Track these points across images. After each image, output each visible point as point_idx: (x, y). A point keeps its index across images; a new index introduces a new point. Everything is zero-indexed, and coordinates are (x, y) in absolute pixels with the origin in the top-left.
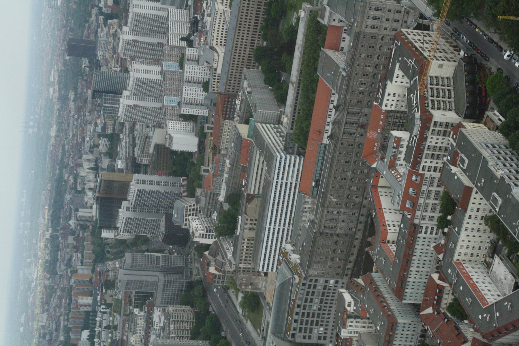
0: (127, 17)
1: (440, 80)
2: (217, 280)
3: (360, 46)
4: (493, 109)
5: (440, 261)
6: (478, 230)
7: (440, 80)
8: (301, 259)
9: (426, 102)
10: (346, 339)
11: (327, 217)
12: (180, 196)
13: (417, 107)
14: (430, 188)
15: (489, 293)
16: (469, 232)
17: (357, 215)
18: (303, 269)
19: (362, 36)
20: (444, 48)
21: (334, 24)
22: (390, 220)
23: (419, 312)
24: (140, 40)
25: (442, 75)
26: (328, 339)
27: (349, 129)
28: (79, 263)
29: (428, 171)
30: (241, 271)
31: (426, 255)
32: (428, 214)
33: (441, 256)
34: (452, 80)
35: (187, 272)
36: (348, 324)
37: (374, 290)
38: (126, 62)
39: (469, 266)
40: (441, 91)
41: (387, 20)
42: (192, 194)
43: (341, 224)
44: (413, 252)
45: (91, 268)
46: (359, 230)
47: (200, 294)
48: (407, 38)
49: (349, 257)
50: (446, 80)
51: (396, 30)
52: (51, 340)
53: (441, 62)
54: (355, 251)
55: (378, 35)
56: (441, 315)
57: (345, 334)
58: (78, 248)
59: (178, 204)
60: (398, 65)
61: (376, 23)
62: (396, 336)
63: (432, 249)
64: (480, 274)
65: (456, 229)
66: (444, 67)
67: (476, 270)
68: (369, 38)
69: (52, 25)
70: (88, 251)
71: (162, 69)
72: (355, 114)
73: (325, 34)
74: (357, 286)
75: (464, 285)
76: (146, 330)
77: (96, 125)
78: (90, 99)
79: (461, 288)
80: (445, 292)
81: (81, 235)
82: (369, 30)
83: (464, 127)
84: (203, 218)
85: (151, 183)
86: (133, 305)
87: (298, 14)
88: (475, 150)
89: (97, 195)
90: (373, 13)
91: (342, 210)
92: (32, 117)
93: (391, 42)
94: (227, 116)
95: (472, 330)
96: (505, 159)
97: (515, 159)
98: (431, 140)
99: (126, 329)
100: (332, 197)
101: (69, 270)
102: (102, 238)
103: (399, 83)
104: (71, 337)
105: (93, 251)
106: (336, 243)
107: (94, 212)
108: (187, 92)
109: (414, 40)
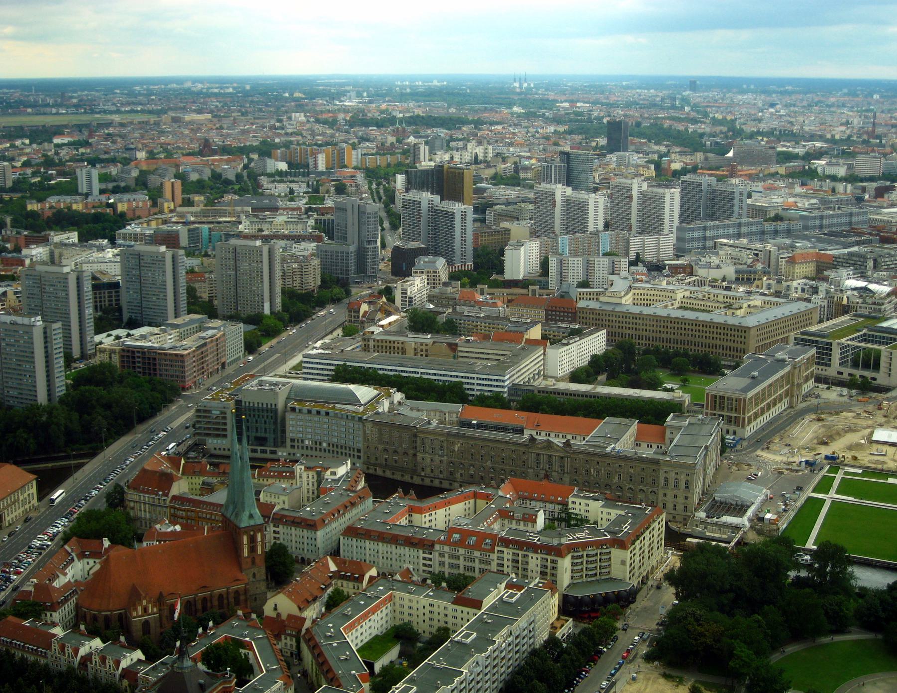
0: (659, 186)
1: (607, 564)
2: (353, 314)
3: (643, 466)
4: (575, 626)
5: (392, 577)
6: (431, 619)
7: (607, 564)
8: (383, 413)
9: (580, 549)
10: (292, 473)
11: (435, 441)
12: (450, 262)
13: (574, 539)
14: (477, 561)
15: (358, 634)
16: (428, 608)
17: (441, 476)
18: (372, 416)
19: (654, 467)
20: (645, 566)
21: (668, 433)
22: (437, 516)
23: (331, 555)
24: (633, 203)
25: (612, 565)
26: (291, 451)
27: (544, 459)
28: (364, 152)
29: (498, 557)
30: (365, 343)
31: (398, 561)
32: (447, 560)
33: (398, 577)
34: (607, 577)
35: (360, 278)
36: (311, 474)
37: (353, 502)
38: (605, 189)
39: (388, 611)
40: (594, 566)
41: (675, 496)
42: (453, 277)
43: (428, 458)
44: (401, 544)
45: (360, 166)
46: (422, 480)
47: (335, 296)
48: (654, 521)
49: (390, 470)
50: (607, 570)
51: (664, 507)
52: (275, 129)
53: (628, 563)
54: (398, 477)
55: (657, 487)
56: (329, 581)
57: (298, 471)
58: (383, 150)
59: (441, 262)
60: (623, 513)
61: (672, 483)
62: (301, 530)
63: (405, 568)
64: (380, 623)
65: (431, 594)
66: (622, 567)
67: (385, 619)
68: (653, 476)
69: (641, 102)
70: (381, 161)
71: (600, 232)
72: (562, 467)
73: (655, 424)
74: (356, 481)
75: (366, 606)
76: (289, 235)
77: (529, 158)
78: (559, 149)
79: (362, 603)
80: (356, 584)
81: (397, 151)
82: (662, 476)
83: (552, 595)
84: (425, 293)
85: (464, 228)
86: (319, 217)
87: (677, 389)
88: (525, 610)
89: (446, 166)
90: (683, 478)
91: (445, 458)
92: (532, 85)
93: (650, 503)
94: (550, 313)
95: (315, 617)
96: (517, 645)
97: (518, 655)
98: (535, 558)
99: (290, 213)
100: (459, 445)
101: (356, 141)
102: (394, 175)
103: (600, 516)
104: (279, 151)
105: (380, 166)
106: (405, 453)
107: (426, 164)
108: (576, 262)
109: (653, 529)
